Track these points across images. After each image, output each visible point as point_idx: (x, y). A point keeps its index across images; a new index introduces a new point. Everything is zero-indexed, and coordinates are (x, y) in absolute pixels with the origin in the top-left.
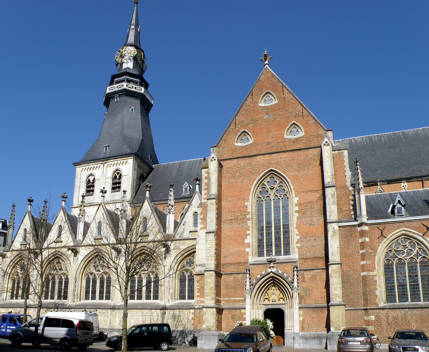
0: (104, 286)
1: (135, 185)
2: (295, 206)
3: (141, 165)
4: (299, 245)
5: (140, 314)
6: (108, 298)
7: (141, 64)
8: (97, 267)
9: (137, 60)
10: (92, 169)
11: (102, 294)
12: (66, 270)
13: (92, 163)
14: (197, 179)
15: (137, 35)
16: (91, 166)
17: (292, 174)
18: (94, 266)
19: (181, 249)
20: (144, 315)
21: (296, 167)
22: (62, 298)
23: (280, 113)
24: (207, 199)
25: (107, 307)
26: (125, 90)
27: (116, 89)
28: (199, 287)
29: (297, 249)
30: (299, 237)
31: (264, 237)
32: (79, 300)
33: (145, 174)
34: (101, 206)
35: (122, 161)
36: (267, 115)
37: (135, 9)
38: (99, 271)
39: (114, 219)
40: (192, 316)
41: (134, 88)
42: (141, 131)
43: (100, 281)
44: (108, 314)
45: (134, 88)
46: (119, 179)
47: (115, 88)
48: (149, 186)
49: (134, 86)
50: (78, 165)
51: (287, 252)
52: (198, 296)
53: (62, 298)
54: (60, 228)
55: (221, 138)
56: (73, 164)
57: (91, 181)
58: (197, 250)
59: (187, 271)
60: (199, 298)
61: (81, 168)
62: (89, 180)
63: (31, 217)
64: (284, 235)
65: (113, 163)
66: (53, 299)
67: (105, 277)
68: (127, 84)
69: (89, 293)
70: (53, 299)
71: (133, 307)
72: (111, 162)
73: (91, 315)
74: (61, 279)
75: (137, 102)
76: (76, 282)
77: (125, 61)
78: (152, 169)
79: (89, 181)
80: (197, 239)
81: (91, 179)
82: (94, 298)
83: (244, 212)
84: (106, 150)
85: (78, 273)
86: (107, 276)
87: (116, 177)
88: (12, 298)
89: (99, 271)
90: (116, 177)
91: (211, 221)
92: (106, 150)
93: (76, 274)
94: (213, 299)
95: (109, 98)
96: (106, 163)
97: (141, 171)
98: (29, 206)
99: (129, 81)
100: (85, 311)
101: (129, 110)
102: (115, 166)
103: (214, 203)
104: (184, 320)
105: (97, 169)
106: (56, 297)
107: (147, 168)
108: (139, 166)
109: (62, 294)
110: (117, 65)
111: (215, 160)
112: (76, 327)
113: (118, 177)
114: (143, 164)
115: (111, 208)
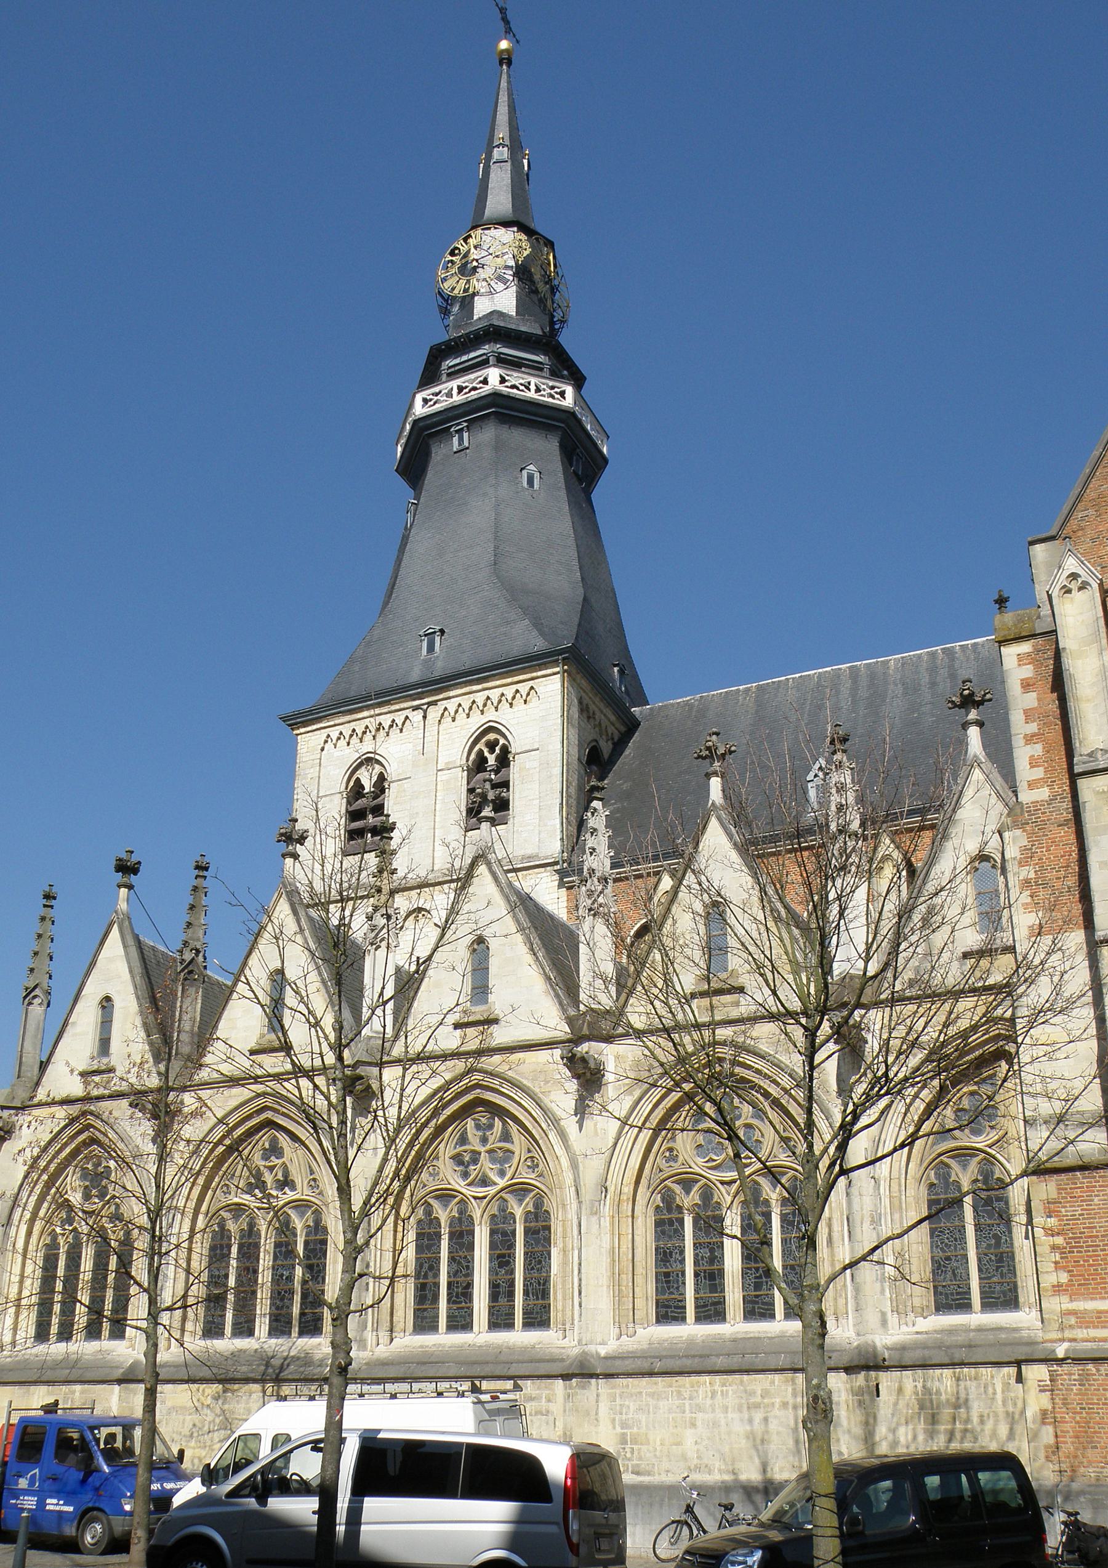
0: (512, 1256)
1: (573, 790)
3: (592, 707)
5: (732, 1400)
6: (538, 1318)
7: (548, 295)
8: (475, 1160)
9: (533, 282)
11: (503, 1301)
13: (368, 708)
14: (968, 701)
15: (520, 183)
18: (457, 1159)
20: (757, 1406)
22: (295, 1330)
25: (543, 1369)
26: (496, 397)
27: (457, 399)
28: (1059, 1240)
32: (384, 1336)
33: (606, 748)
35: (509, 692)
37: (504, 84)
38: (485, 1182)
40: (1036, 1402)
41: (533, 387)
42: (576, 562)
43: (493, 1232)
44: (552, 1407)
45: (533, 387)
46: (497, 772)
47: (449, 393)
48: (721, 751)
49: (533, 381)
50: (305, 724)
53: (295, 1330)
55: (1079, 498)
56: (284, 719)
59: (964, 1154)
60: (1065, 1299)
62: (359, 784)
63: (131, 941)
65: (466, 702)
66: (250, 1333)
67: (518, 1211)
69: (436, 1298)
70: (250, 1333)
71: (688, 1363)
72: (456, 699)
73: (498, 1412)
74: (285, 1228)
75: (549, 446)
77: (482, 287)
78: (632, 725)
79: (357, 791)
82: (461, 1322)
84: (431, 648)
86: (529, 1202)
87: (485, 760)
88: (42, 1335)
89: (485, 1182)
90: (481, 760)
92: (431, 648)
95: (426, 435)
96: (435, 703)
98: (124, 891)
100: (475, 1390)
101: (516, 481)
102: (476, 712)
104: (989, 1426)
105: (395, 731)
106: (262, 1326)
107: (613, 718)
108: (584, 709)
109: (296, 1310)
110: (445, 312)
111: (1083, 587)
112: (558, 1497)
113: (491, 759)
114: (597, 700)
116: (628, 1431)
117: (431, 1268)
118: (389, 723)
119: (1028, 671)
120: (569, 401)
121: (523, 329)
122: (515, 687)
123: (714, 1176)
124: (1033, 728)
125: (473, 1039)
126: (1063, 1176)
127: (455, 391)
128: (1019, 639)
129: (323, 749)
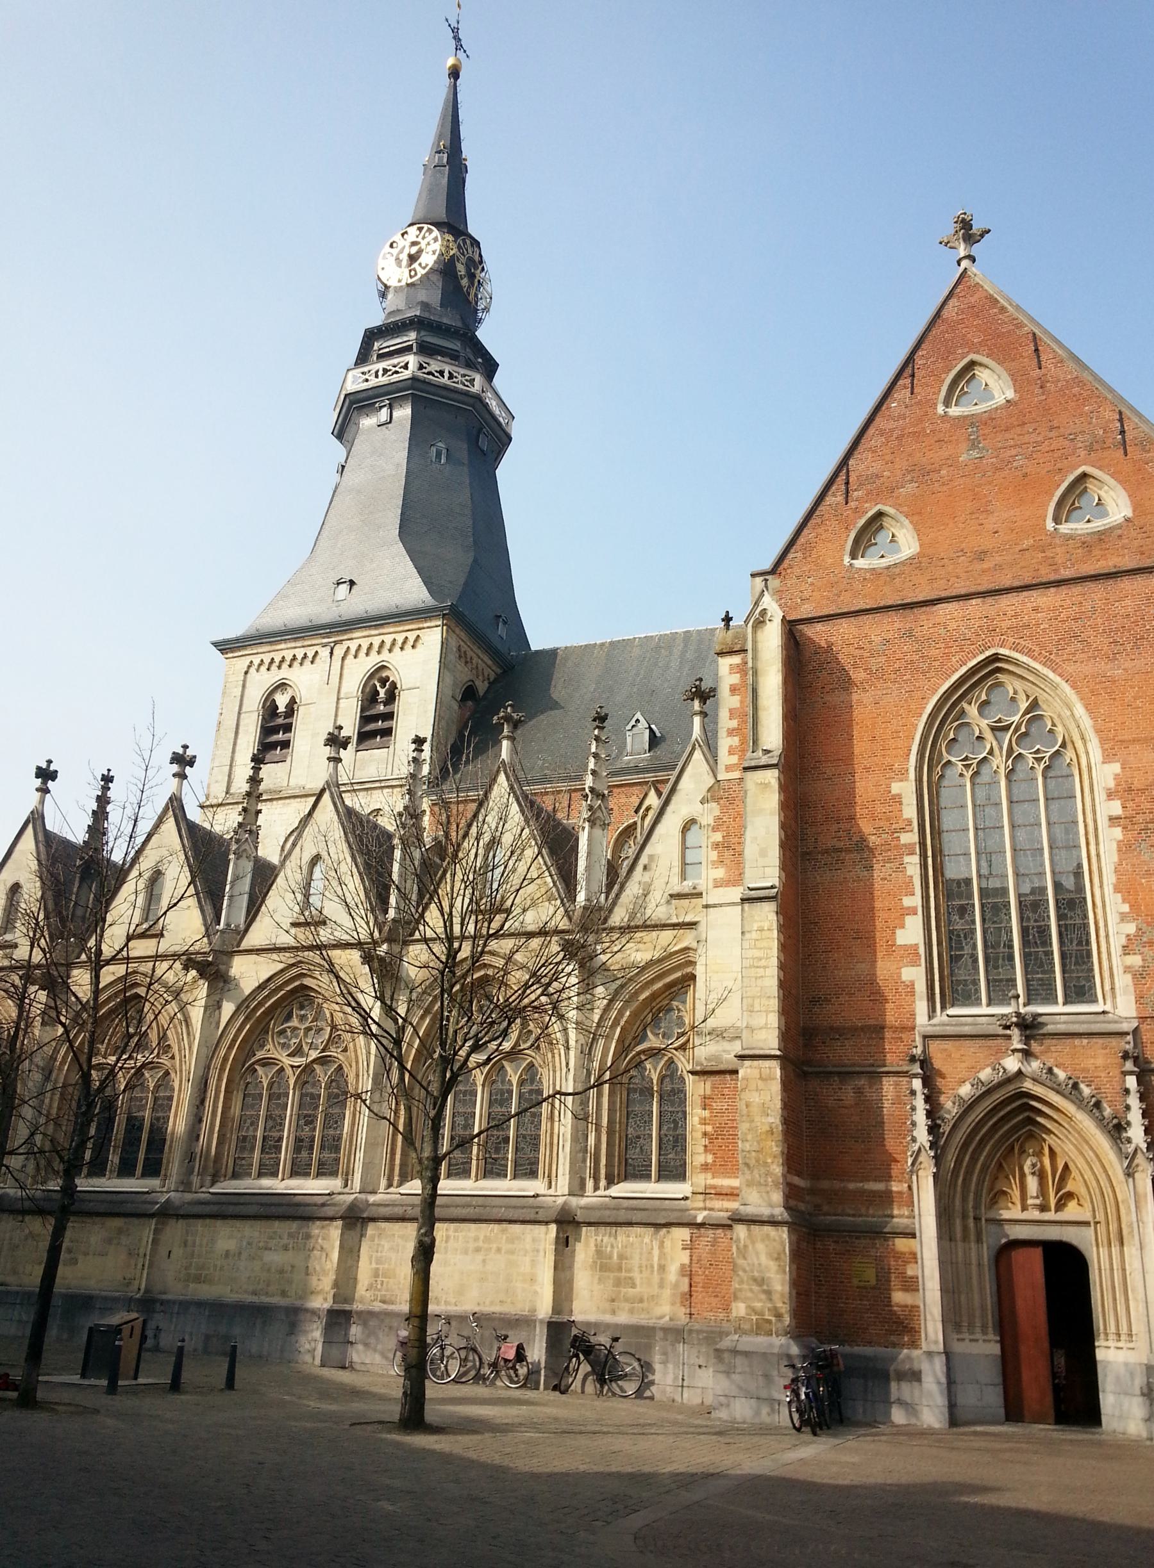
2: (1104, 796)
3: (470, 653)
4: (1135, 960)
10: (285, 666)
16: (284, 653)
17: (1087, 669)
21: (1101, 642)
23: (1026, 438)
24: (746, 769)
27: (383, 380)
28: (709, 1128)
29: (1124, 981)
30: (1131, 928)
31: (973, 922)
34: (326, 796)
36: (974, 446)
39: (368, 843)
41: (446, 375)
45: (446, 375)
49: (447, 369)
51: (1080, 991)
52: (705, 1167)
56: (215, 644)
58: (699, 971)
60: (709, 1175)
61: (245, 662)
64: (1060, 917)
68: (422, 359)
72: (359, 639)
79: (270, 709)
80: (702, 927)
81: (282, 701)
83: (888, 820)
85: (217, 1062)
87: (378, 693)
91: (763, 853)
97: (464, 674)
102: (374, 653)
103: (775, 784)
107: (490, 662)
108: (462, 655)
113: (382, 693)
114: (475, 648)
115: (362, 803)
116: (381, 1267)
117: (252, 1124)
118: (302, 655)
119: (735, 679)
120: (476, 388)
121: (445, 321)
122: (404, 635)
124: (734, 724)
125: (304, 936)
126: (717, 1078)
128: (731, 653)
129: (246, 673)
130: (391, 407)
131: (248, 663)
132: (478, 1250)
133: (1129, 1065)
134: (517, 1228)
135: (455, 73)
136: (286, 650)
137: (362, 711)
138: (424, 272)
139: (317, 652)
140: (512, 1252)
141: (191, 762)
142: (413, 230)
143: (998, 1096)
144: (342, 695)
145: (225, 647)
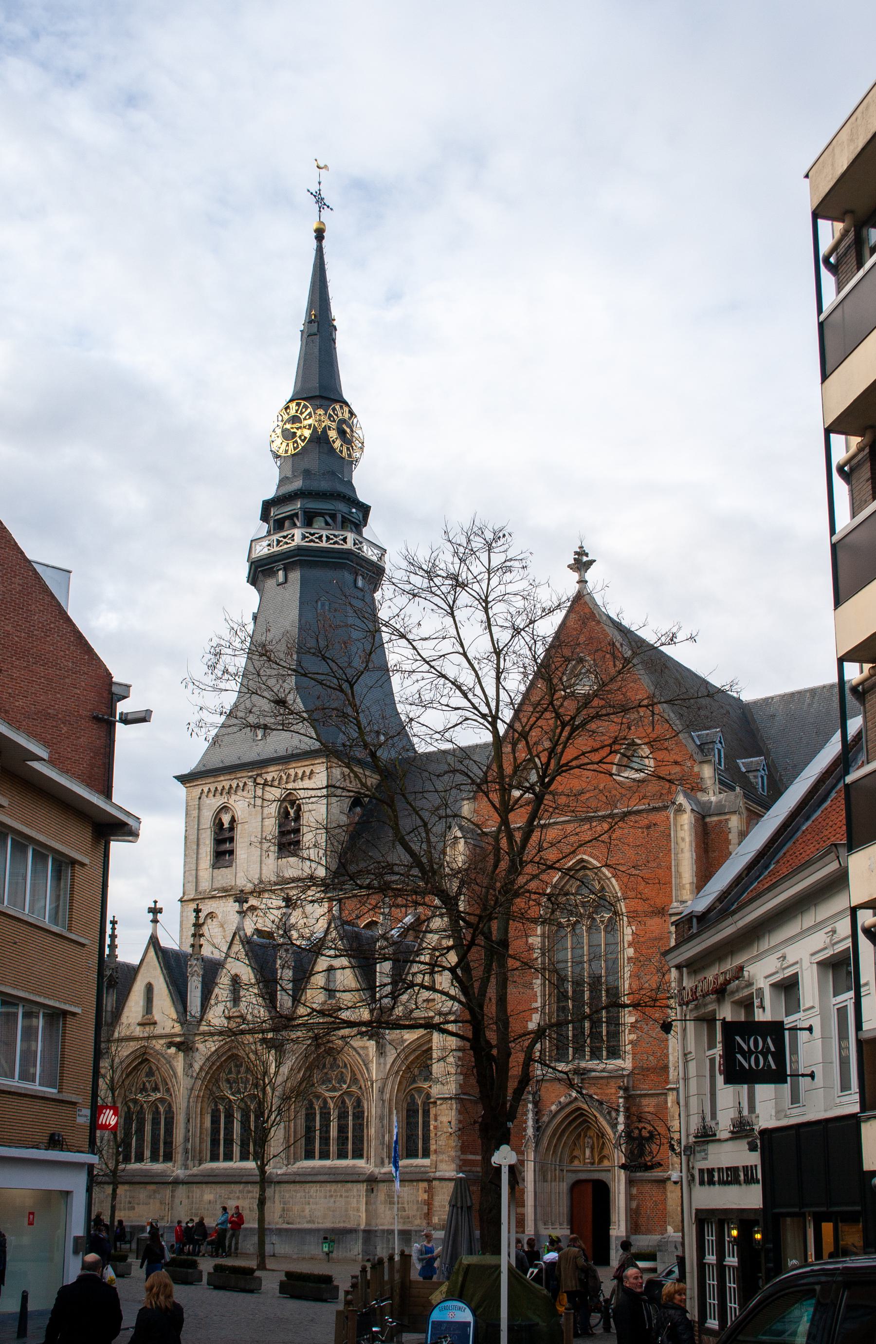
12: (168, 1090)
16: (224, 783)
19: (406, 1040)
22: (161, 1159)
26: (299, 550)
49: (324, 533)
54: (149, 988)
57: (226, 825)
68: (303, 530)
71: (234, 1179)
74: (157, 1112)
76: (189, 1121)
79: (218, 825)
82: (228, 1157)
93: (189, 1102)
94: (453, 1161)
99: (309, 520)
120: (349, 545)
122: (302, 769)
123: (327, 1094)
127: (275, 543)
129: (200, 798)
130: (286, 570)
131: (200, 791)
132: (331, 1196)
133: (621, 1093)
134: (349, 1185)
135: (320, 235)
136: (224, 782)
137: (280, 826)
138: (303, 444)
139: (245, 783)
140: (347, 1197)
141: (160, 911)
142: (293, 405)
143: (568, 1110)
144: (265, 816)
145: (183, 779)
